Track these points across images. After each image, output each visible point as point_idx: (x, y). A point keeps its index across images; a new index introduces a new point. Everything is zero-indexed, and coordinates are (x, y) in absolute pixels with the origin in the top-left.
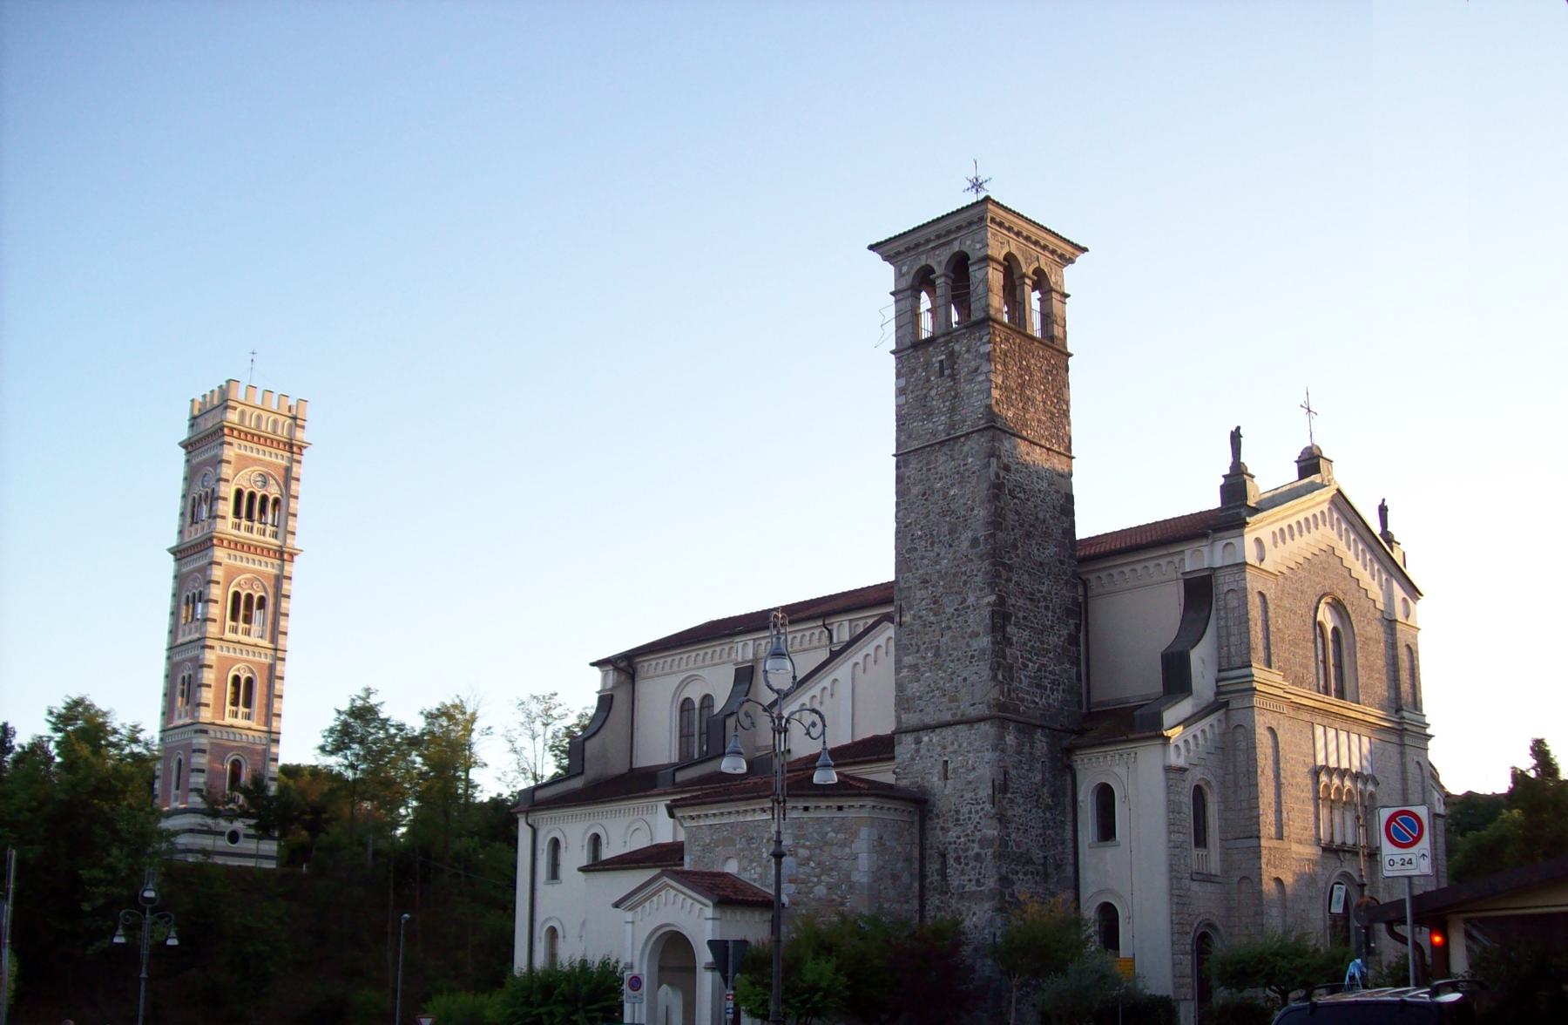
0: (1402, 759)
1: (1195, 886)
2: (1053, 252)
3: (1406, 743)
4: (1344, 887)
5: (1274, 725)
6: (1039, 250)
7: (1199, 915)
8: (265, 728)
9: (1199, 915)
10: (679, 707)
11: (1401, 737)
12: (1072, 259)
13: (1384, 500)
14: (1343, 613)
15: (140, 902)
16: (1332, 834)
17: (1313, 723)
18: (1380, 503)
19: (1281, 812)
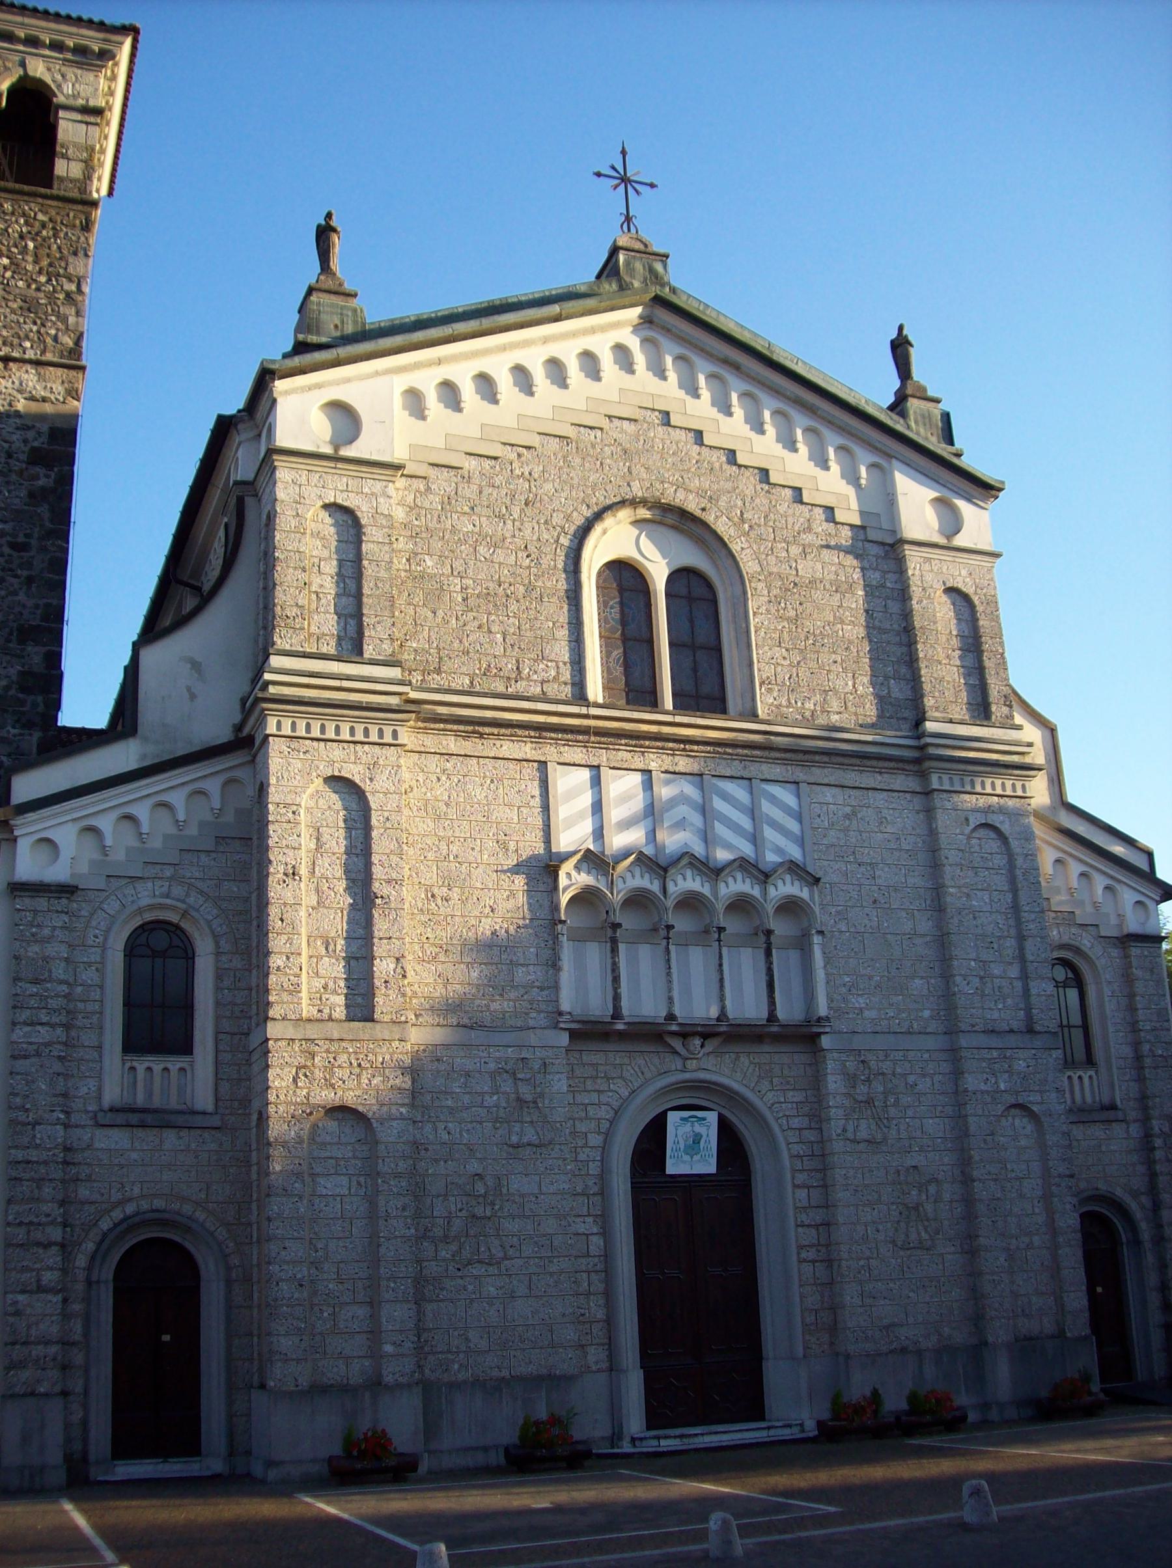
0: (930, 824)
1: (117, 1139)
2: (57, 46)
3: (935, 785)
4: (712, 1117)
5: (353, 772)
6: (21, 48)
7: (121, 1203)
8: (923, 1121)
9: (121, 1203)
10: (132, 929)
11: (924, 775)
12: (109, 51)
13: (901, 328)
14: (708, 537)
15: (968, 1483)
16: (617, 998)
17: (543, 765)
18: (894, 335)
19: (369, 958)
